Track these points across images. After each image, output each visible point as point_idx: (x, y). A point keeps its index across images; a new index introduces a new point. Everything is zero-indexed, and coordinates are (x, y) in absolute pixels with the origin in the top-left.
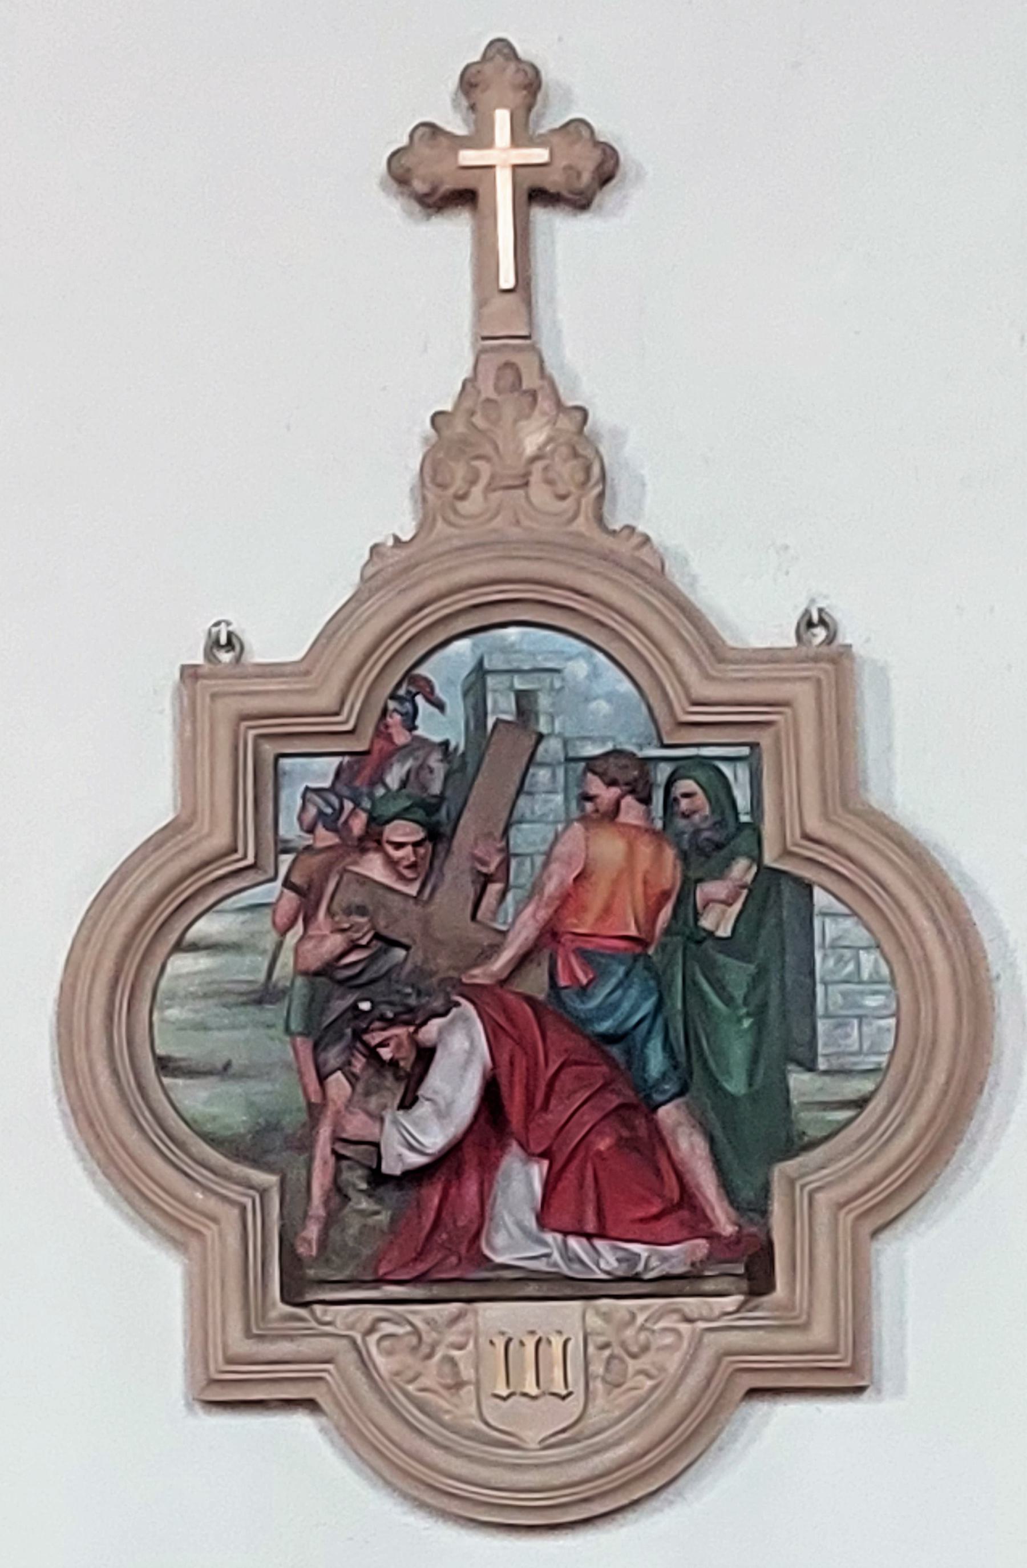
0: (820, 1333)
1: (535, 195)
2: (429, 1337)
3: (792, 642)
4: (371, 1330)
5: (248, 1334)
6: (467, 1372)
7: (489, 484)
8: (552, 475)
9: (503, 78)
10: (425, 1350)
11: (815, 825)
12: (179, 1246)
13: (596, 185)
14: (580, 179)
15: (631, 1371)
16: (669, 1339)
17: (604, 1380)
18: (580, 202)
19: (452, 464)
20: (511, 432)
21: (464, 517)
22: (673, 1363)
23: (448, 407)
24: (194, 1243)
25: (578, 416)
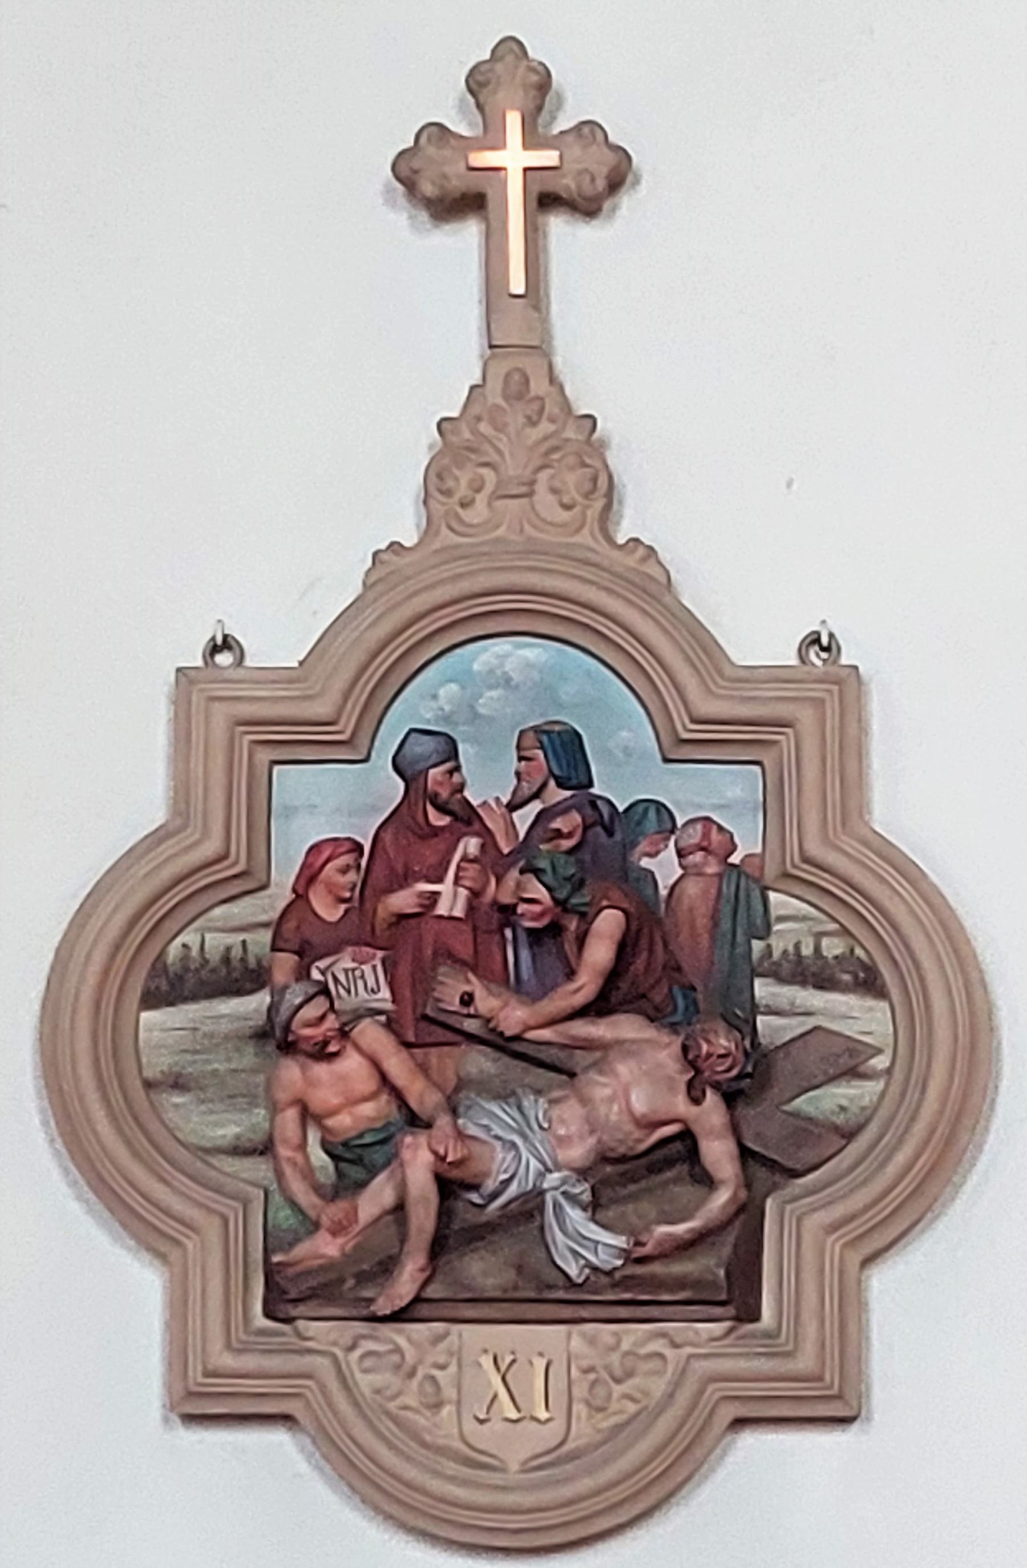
0: (805, 1362)
1: (546, 201)
2: (410, 1355)
3: (794, 661)
4: (352, 1348)
5: (228, 1346)
6: (449, 1392)
7: (493, 493)
8: (557, 484)
9: (511, 79)
10: (406, 1368)
11: (815, 848)
12: (162, 1257)
13: (606, 192)
14: (588, 186)
15: (615, 1395)
16: (655, 1364)
17: (588, 1404)
18: (587, 208)
19: (457, 472)
20: (522, 439)
21: (471, 526)
22: (658, 1387)
23: (455, 414)
24: (175, 1255)
25: (588, 423)
